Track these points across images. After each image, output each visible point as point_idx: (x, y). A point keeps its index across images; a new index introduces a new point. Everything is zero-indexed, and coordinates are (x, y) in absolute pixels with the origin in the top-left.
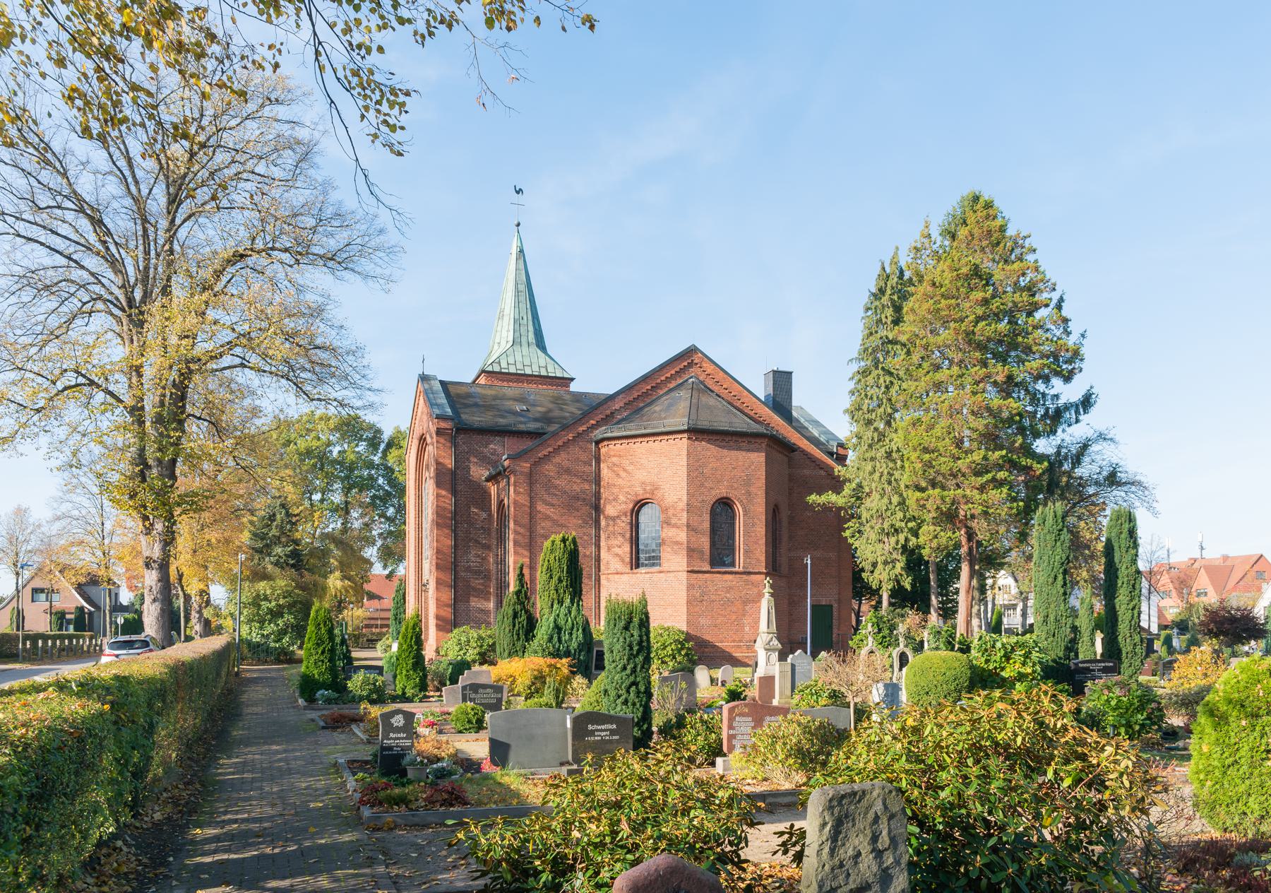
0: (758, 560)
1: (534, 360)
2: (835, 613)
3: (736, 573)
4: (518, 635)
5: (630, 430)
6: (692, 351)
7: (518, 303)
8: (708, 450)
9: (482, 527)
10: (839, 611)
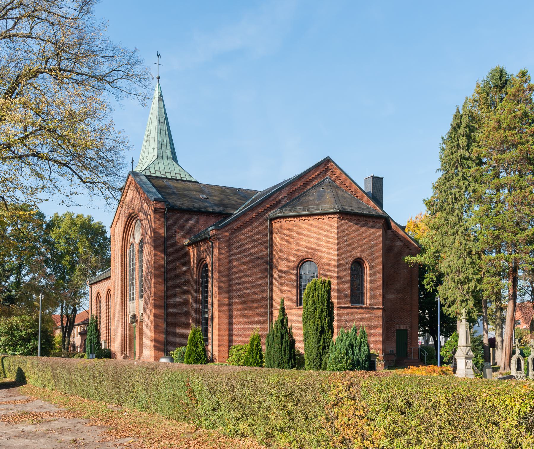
0: (378, 299)
1: (172, 169)
2: (409, 335)
3: (366, 308)
4: (285, 351)
5: (297, 211)
6: (328, 160)
7: (160, 130)
8: (350, 226)
10: (411, 334)
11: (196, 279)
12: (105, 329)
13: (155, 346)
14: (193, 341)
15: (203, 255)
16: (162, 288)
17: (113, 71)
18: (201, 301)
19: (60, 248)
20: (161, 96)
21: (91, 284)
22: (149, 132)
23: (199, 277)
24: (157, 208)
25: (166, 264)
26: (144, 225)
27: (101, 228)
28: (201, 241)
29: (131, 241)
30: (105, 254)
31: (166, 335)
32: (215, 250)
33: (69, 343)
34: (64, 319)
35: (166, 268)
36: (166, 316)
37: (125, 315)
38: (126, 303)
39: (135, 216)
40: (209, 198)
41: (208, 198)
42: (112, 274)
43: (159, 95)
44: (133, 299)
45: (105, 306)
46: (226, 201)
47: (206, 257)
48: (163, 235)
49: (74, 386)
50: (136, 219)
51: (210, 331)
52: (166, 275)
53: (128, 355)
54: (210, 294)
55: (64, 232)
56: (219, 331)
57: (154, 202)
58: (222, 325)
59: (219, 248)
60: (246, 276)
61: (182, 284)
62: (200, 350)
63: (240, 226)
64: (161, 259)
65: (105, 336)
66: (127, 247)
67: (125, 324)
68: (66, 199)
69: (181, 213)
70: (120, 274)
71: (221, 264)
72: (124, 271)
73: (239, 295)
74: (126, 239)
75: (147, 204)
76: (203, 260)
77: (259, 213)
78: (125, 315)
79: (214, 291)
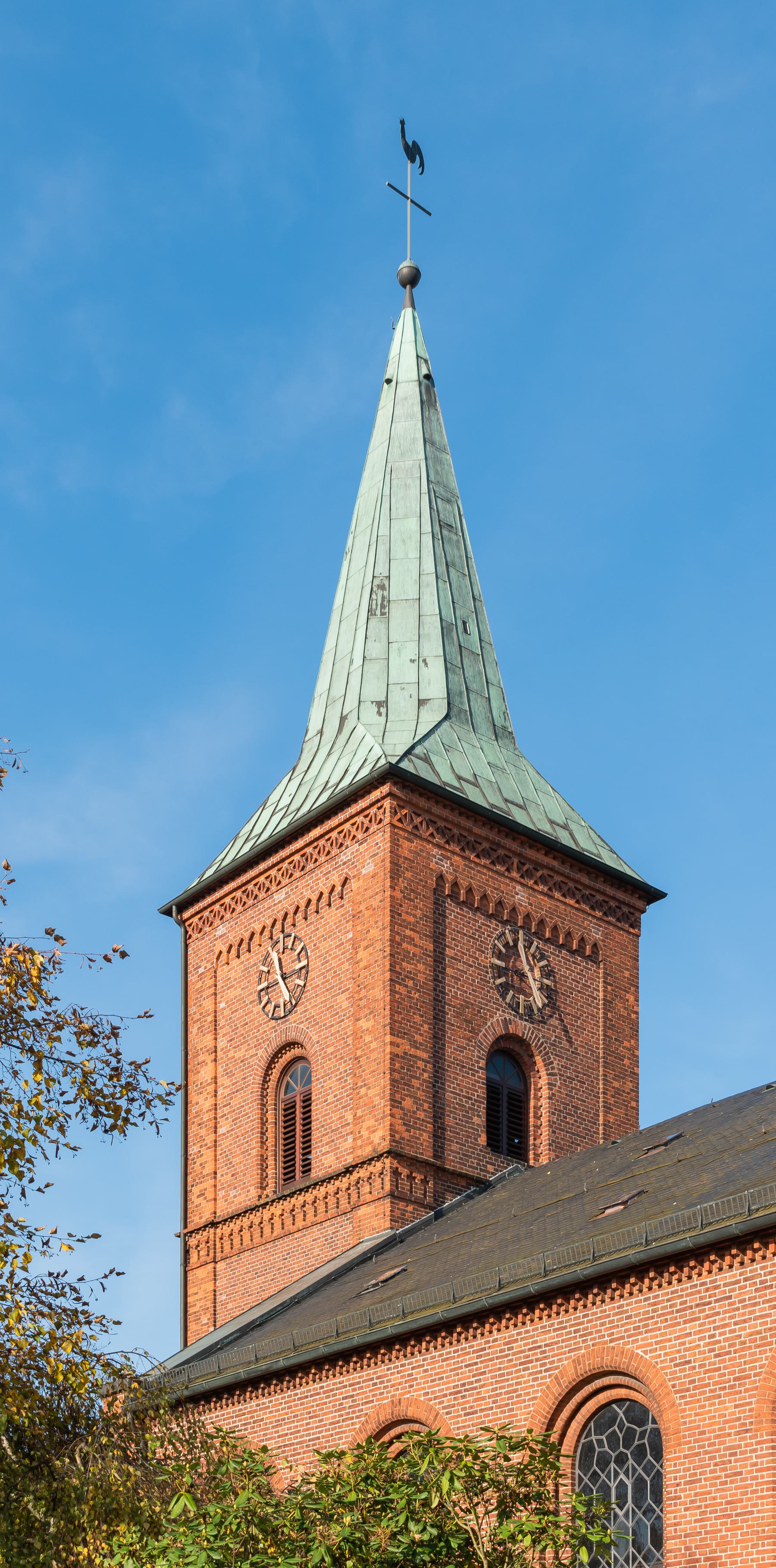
22: (382, 570)
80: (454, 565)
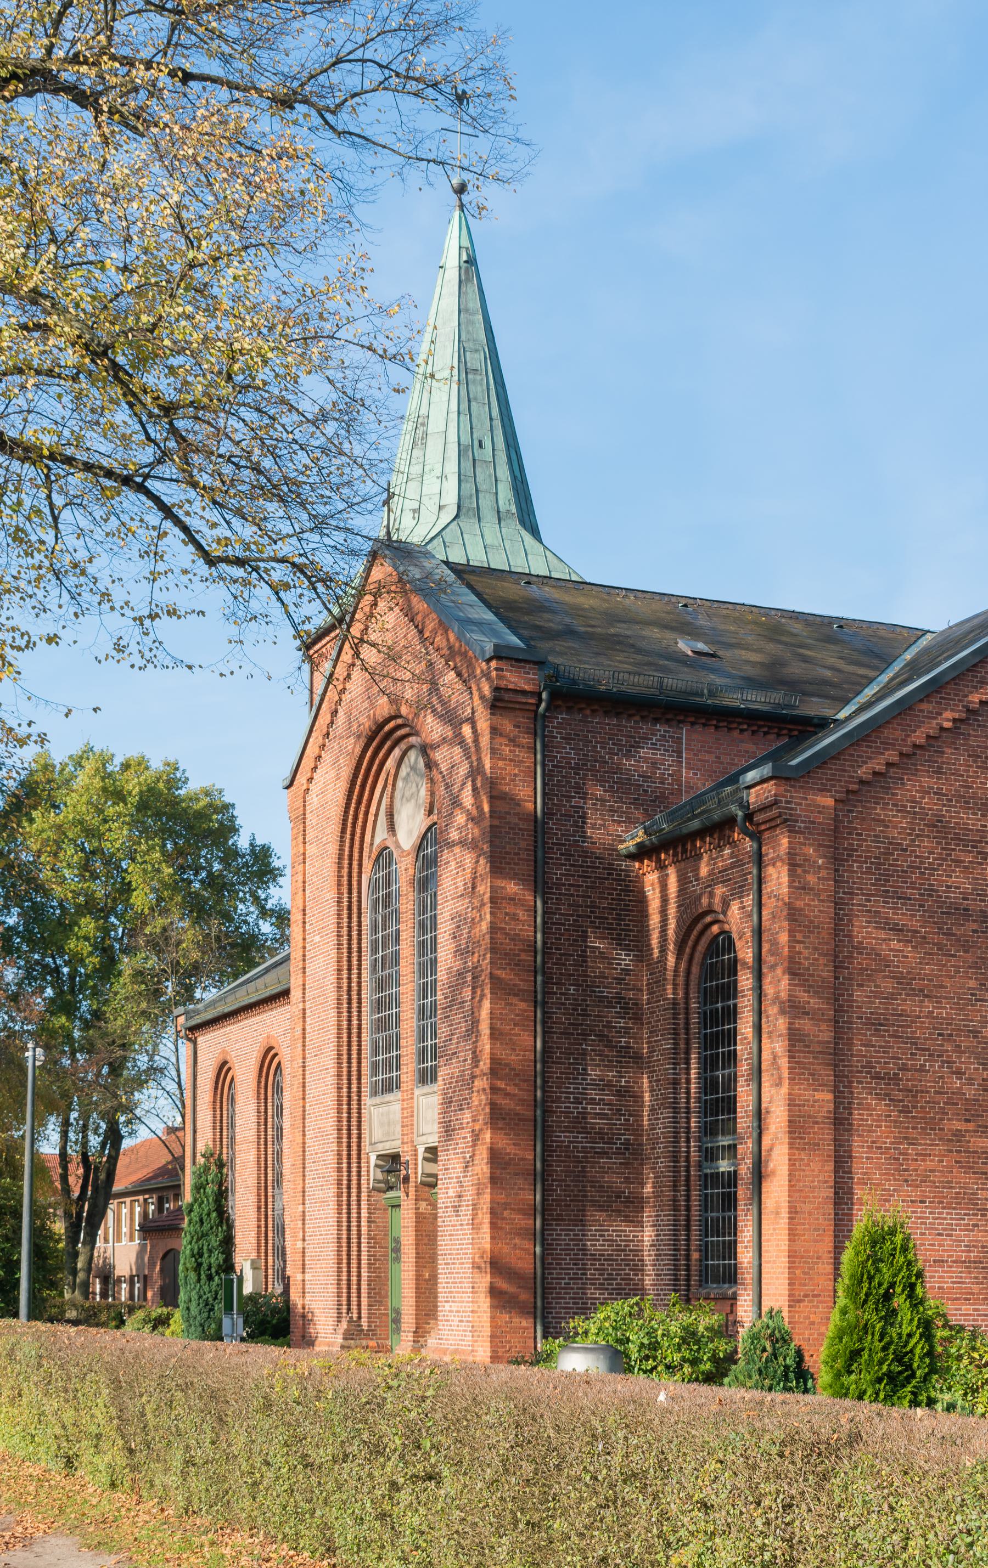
7: (467, 402)
9: (619, 998)
11: (675, 1003)
12: (252, 1213)
13: (494, 1292)
14: (871, 1278)
15: (711, 895)
16: (526, 1038)
17: (339, 61)
18: (699, 1100)
19: (58, 890)
20: (470, 263)
21: (192, 1029)
22: (424, 411)
23: (687, 993)
24: (508, 690)
25: (544, 933)
26: (444, 767)
27: (217, 810)
28: (700, 834)
29: (377, 841)
30: (227, 917)
31: (543, 1245)
32: (771, 871)
33: (89, 1269)
34: (71, 1167)
35: (544, 953)
36: (544, 1161)
37: (354, 1153)
38: (354, 1103)
39: (399, 733)
40: (720, 653)
41: (712, 655)
42: (295, 984)
43: (464, 258)
44: (388, 1087)
45: (254, 1119)
46: (795, 670)
47: (726, 904)
48: (530, 806)
49: (237, 1482)
50: (403, 746)
51: (746, 1234)
52: (544, 982)
53: (364, 1323)
54: (743, 1068)
55: (74, 823)
56: (793, 1235)
57: (493, 664)
58: (807, 1207)
59: (794, 864)
60: (915, 993)
61: (609, 1025)
62: (906, 1330)
63: (883, 768)
64: (522, 914)
65: (254, 1241)
66: (360, 865)
67: (354, 1191)
68: (131, 634)
69: (606, 713)
70: (333, 978)
71: (799, 937)
72: (349, 969)
73: (877, 1077)
74: (358, 831)
75: (459, 675)
76: (708, 919)
77: (969, 711)
78: (354, 1153)
79: (766, 1055)
80: (476, 399)
